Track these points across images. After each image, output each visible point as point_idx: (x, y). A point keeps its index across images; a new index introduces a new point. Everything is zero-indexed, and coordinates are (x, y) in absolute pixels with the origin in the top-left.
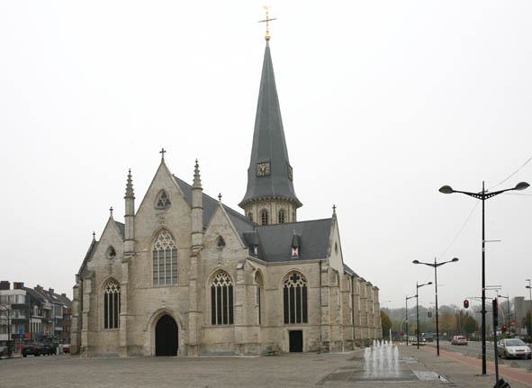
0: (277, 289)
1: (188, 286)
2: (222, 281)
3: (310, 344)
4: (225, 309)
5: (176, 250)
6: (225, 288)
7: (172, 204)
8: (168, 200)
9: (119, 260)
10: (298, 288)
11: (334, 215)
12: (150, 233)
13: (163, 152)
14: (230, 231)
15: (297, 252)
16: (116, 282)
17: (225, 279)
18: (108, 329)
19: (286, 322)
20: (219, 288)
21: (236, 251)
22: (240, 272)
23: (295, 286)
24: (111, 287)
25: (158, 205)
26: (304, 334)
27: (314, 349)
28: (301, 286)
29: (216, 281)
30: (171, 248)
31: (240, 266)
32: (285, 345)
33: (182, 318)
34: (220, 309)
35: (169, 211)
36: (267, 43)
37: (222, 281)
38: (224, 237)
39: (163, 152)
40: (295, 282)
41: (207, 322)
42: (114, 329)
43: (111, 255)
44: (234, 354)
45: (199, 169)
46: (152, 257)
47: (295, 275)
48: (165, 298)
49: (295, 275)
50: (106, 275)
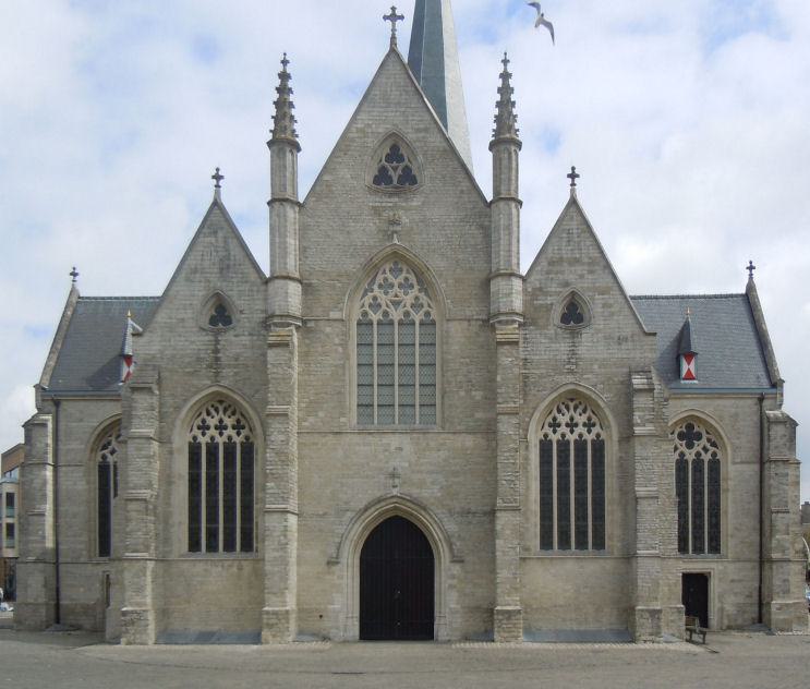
2: (572, 425)
3: (730, 609)
4: (581, 504)
5: (433, 323)
8: (407, 170)
10: (698, 463)
11: (751, 287)
12: (352, 265)
13: (74, 274)
16: (230, 407)
17: (581, 419)
20: (563, 445)
21: (620, 340)
24: (212, 422)
25: (377, 180)
26: (97, 552)
27: (740, 622)
28: (706, 457)
30: (417, 317)
34: (564, 504)
37: (572, 425)
40: (690, 446)
43: (213, 321)
45: (512, 83)
46: (354, 341)
47: (690, 427)
48: (400, 464)
49: (690, 427)
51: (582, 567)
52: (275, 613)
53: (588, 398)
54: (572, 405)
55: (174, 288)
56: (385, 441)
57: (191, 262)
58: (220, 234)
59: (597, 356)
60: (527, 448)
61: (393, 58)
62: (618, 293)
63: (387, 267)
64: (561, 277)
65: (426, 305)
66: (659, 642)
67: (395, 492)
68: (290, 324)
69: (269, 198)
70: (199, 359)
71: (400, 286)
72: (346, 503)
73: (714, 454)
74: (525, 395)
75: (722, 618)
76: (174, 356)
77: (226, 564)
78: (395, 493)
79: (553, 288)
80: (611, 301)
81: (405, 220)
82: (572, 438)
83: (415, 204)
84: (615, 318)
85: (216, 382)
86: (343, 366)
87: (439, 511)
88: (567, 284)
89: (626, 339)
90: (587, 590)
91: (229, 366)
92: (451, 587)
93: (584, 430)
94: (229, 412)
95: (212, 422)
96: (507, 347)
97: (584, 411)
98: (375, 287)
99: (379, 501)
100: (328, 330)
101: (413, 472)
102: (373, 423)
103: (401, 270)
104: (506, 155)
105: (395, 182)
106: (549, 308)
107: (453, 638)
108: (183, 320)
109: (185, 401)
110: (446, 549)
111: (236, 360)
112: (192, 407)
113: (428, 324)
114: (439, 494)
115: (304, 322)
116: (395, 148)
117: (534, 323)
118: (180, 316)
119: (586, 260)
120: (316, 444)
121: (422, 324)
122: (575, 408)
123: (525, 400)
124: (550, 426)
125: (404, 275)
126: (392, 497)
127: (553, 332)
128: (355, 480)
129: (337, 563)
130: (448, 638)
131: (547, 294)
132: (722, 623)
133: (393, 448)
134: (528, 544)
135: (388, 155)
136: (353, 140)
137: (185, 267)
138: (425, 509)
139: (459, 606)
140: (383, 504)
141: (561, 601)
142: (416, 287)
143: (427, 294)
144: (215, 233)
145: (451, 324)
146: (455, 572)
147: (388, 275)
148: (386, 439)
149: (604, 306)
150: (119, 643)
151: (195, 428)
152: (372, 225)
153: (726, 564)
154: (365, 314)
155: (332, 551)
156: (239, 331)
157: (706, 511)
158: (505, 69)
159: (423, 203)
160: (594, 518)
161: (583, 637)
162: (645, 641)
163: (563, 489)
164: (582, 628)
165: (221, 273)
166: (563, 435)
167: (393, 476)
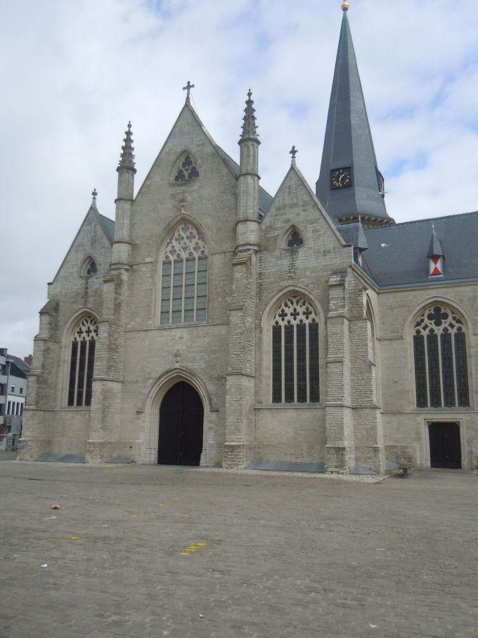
0: (401, 338)
1: (227, 323)
2: (295, 314)
5: (206, 258)
6: (301, 327)
7: (201, 174)
8: (194, 169)
9: (101, 280)
10: (446, 336)
12: (158, 229)
13: (189, 87)
14: (314, 214)
15: (439, 266)
17: (301, 310)
18: (72, 408)
19: (421, 402)
21: (325, 253)
22: (335, 293)
23: (439, 331)
24: (84, 329)
25: (177, 178)
28: (453, 332)
29: (283, 315)
30: (196, 255)
31: (334, 279)
32: (422, 452)
33: (211, 388)
35: (196, 186)
37: (295, 314)
38: (301, 227)
39: (189, 87)
40: (438, 324)
41: (263, 399)
42: (84, 407)
44: (322, 469)
47: (437, 310)
48: (181, 347)
49: (437, 310)
50: (79, 308)
51: (300, 415)
52: (93, 444)
53: (304, 295)
54: (294, 300)
55: (69, 257)
56: (173, 333)
57: (78, 241)
58: (93, 224)
59: (309, 266)
60: (261, 332)
61: (187, 109)
62: (324, 221)
63: (180, 228)
64: (284, 217)
65: (202, 247)
66: (342, 474)
67: (177, 365)
68: (121, 268)
69: (116, 198)
70: (78, 294)
71: (188, 238)
72: (149, 374)
73: (460, 329)
74: (260, 297)
75: (471, 460)
76: (66, 293)
77: (83, 413)
78: (176, 367)
79: (279, 224)
80: (319, 228)
81: (189, 198)
82: (295, 323)
83: (194, 188)
84: (321, 239)
85: (85, 306)
86: (151, 290)
87: (203, 377)
88: (288, 221)
89: (329, 252)
90: (303, 432)
91: (92, 296)
92: (211, 428)
93: (291, 318)
94: (93, 323)
95: (84, 329)
96: (239, 266)
97: (304, 304)
98: (174, 241)
99: (168, 372)
100: (144, 269)
101: (189, 352)
102: (193, 321)
103: (188, 228)
104: (246, 149)
105: (187, 178)
106: (276, 238)
107: (210, 465)
108: (72, 273)
109: (70, 318)
110: (208, 402)
111: (96, 292)
112: (75, 318)
113: (203, 258)
114: (204, 366)
115: (131, 266)
116: (188, 158)
117: (266, 249)
118: (71, 271)
119: (301, 203)
120: (135, 338)
121: (175, 262)
122: (297, 302)
123: (260, 300)
124: (280, 316)
125: (190, 231)
126: (175, 369)
127: (279, 253)
128: (156, 359)
129: (142, 412)
130: (206, 465)
131: (274, 229)
132: (472, 464)
133: (177, 338)
134: (261, 398)
135: (184, 163)
136: (162, 159)
137: (75, 244)
138: (194, 376)
139: (214, 442)
140: (170, 373)
141: (284, 441)
142: (197, 237)
143: (203, 240)
144: (91, 223)
145: (214, 256)
146: (213, 419)
147: (181, 232)
148: (173, 332)
149: (314, 231)
150: (15, 460)
151: (277, 316)
152: (169, 204)
153: (473, 415)
154: (167, 257)
155: (140, 404)
156: (98, 276)
157: (427, 374)
158: (250, 98)
159: (200, 186)
160: (311, 380)
161: (293, 467)
162: (332, 472)
163: (289, 359)
164: (299, 461)
165: (92, 245)
166: (289, 322)
167: (176, 356)
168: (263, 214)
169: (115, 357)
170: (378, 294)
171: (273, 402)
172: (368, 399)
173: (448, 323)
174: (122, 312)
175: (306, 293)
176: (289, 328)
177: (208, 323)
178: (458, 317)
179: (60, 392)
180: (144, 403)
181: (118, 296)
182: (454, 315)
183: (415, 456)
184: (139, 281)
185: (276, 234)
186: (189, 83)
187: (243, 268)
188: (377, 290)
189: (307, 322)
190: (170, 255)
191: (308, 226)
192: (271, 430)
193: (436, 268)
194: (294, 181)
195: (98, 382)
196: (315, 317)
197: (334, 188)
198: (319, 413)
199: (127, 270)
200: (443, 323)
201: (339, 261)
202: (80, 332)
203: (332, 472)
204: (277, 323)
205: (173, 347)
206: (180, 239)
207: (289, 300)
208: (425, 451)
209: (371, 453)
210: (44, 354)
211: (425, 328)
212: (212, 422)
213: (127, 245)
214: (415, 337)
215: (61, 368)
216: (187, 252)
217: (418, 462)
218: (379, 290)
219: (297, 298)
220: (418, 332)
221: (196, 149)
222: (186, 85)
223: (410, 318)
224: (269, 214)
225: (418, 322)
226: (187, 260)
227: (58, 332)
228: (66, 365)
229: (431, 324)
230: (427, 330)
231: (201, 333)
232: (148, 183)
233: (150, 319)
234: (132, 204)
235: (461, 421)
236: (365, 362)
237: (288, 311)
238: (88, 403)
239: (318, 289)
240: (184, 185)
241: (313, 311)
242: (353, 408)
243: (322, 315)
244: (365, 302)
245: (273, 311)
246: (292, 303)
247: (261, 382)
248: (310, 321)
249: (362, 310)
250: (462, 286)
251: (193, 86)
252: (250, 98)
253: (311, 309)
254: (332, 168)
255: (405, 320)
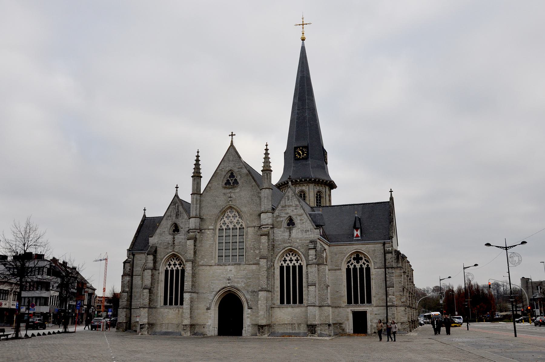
0: (340, 269)
2: (291, 260)
10: (361, 269)
12: (216, 211)
15: (359, 233)
17: (294, 258)
19: (349, 302)
21: (307, 231)
23: (358, 266)
25: (226, 184)
28: (365, 267)
29: (285, 261)
30: (238, 227)
32: (349, 327)
36: (303, 44)
37: (291, 260)
38: (294, 217)
40: (358, 262)
41: (276, 302)
47: (358, 255)
48: (231, 276)
49: (358, 255)
50: (170, 251)
51: (294, 310)
56: (226, 268)
57: (168, 214)
59: (298, 237)
61: (232, 147)
63: (228, 211)
66: (315, 336)
67: (229, 285)
69: (191, 193)
71: (233, 217)
73: (368, 265)
77: (174, 309)
78: (229, 286)
79: (283, 215)
82: (291, 265)
84: (304, 224)
86: (213, 244)
88: (287, 214)
89: (308, 231)
90: (296, 318)
92: (248, 317)
94: (177, 260)
95: (172, 263)
96: (264, 236)
97: (295, 255)
98: (225, 218)
99: (224, 288)
100: (208, 232)
114: (244, 286)
119: (294, 205)
122: (292, 254)
125: (234, 213)
131: (281, 217)
133: (228, 270)
136: (218, 173)
138: (239, 290)
140: (225, 289)
144: (175, 204)
145: (248, 228)
147: (229, 213)
151: (282, 261)
154: (221, 226)
156: (181, 234)
158: (267, 148)
162: (310, 336)
164: (293, 332)
168: (275, 208)
169: (194, 280)
170: (329, 246)
171: (280, 304)
172: (326, 302)
173: (362, 262)
174: (197, 255)
175: (297, 250)
176: (288, 267)
177: (245, 263)
178: (367, 259)
179: (159, 298)
180: (210, 304)
181: (195, 247)
182: (365, 258)
183: (346, 328)
184: (205, 239)
185: (282, 220)
186: (232, 133)
187: (266, 237)
188: (329, 245)
189: (297, 265)
190: (223, 226)
191: (298, 217)
192: (280, 317)
193: (357, 234)
194: (290, 193)
195: (187, 294)
196: (301, 262)
197: (296, 159)
198: (303, 309)
199: (198, 232)
200: (360, 262)
201: (313, 236)
202: (170, 265)
203: (310, 336)
204: (282, 264)
205: (227, 275)
206: (228, 217)
207: (288, 253)
208: (350, 325)
209: (327, 327)
210: (151, 277)
211: (352, 264)
212: (248, 314)
213: (199, 219)
214: (347, 269)
215: (159, 284)
216: (233, 225)
217: (347, 331)
218: (330, 244)
219: (293, 252)
220: (348, 266)
221: (237, 170)
222: (231, 134)
223: (345, 259)
224: (278, 209)
225: (348, 261)
226: (233, 229)
227: (157, 264)
228: (162, 282)
229: (354, 262)
230: (353, 265)
231: (242, 268)
232: (209, 185)
233: (212, 260)
234: (200, 196)
235: (367, 310)
236: (325, 285)
237: (288, 259)
238: (182, 304)
239: (303, 249)
240: (231, 188)
241: (300, 259)
242: (319, 307)
243: (305, 262)
244: (325, 256)
245: (280, 258)
246: (290, 255)
247: (274, 294)
248: (298, 264)
249: (324, 260)
250: (369, 244)
251: (235, 135)
252: (267, 148)
253: (299, 258)
254: (295, 146)
255: (342, 260)
